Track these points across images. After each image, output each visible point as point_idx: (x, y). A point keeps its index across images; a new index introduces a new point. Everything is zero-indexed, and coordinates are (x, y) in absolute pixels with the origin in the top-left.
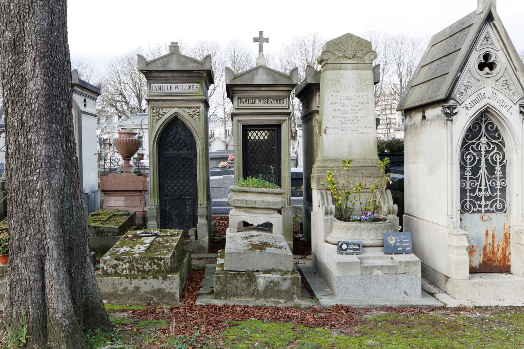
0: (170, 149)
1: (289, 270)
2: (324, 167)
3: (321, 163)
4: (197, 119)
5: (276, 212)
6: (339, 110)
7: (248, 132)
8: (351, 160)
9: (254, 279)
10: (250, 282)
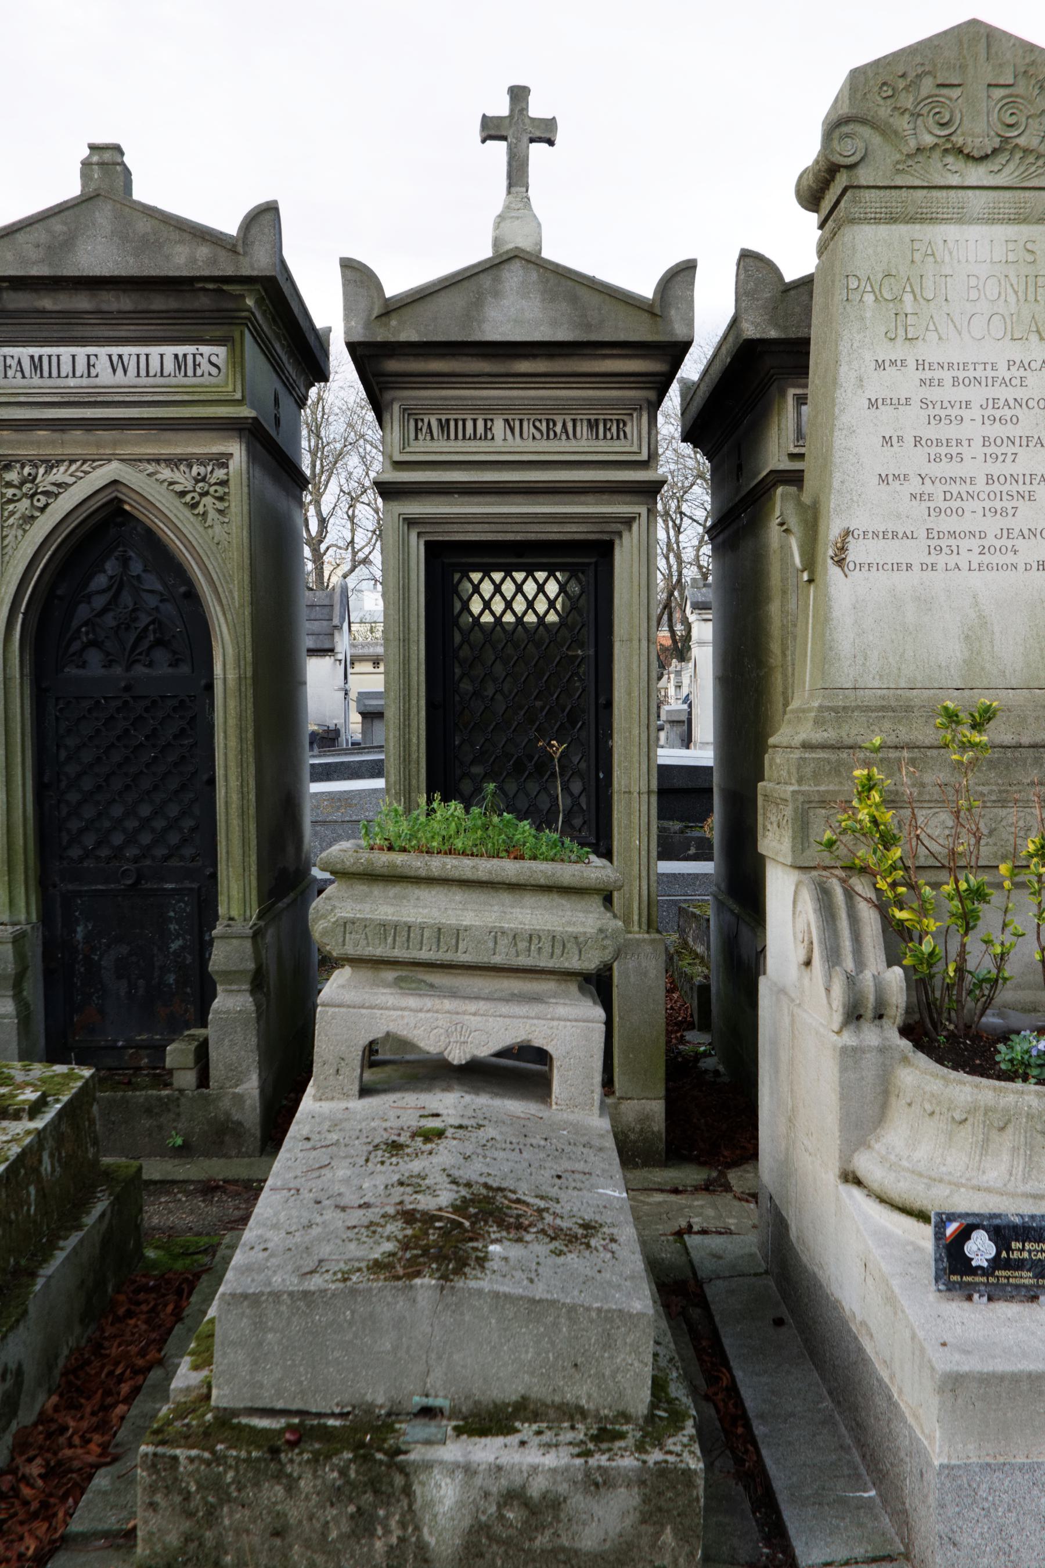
0: (94, 657)
1: (632, 1410)
2: (832, 747)
3: (818, 722)
4: (212, 514)
5: (573, 988)
6: (917, 441)
7: (457, 576)
8: (988, 709)
9: (399, 1480)
10: (369, 1497)
